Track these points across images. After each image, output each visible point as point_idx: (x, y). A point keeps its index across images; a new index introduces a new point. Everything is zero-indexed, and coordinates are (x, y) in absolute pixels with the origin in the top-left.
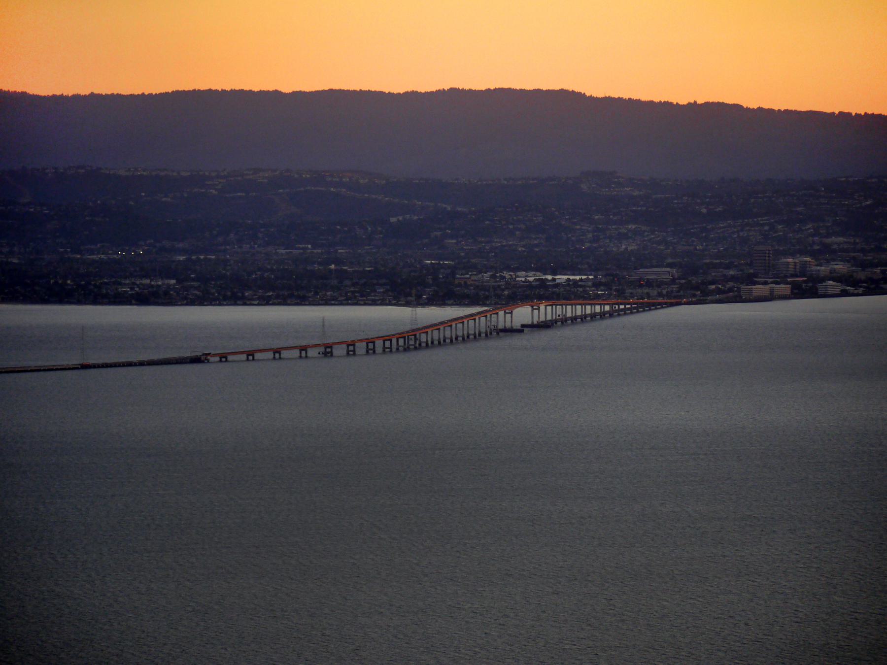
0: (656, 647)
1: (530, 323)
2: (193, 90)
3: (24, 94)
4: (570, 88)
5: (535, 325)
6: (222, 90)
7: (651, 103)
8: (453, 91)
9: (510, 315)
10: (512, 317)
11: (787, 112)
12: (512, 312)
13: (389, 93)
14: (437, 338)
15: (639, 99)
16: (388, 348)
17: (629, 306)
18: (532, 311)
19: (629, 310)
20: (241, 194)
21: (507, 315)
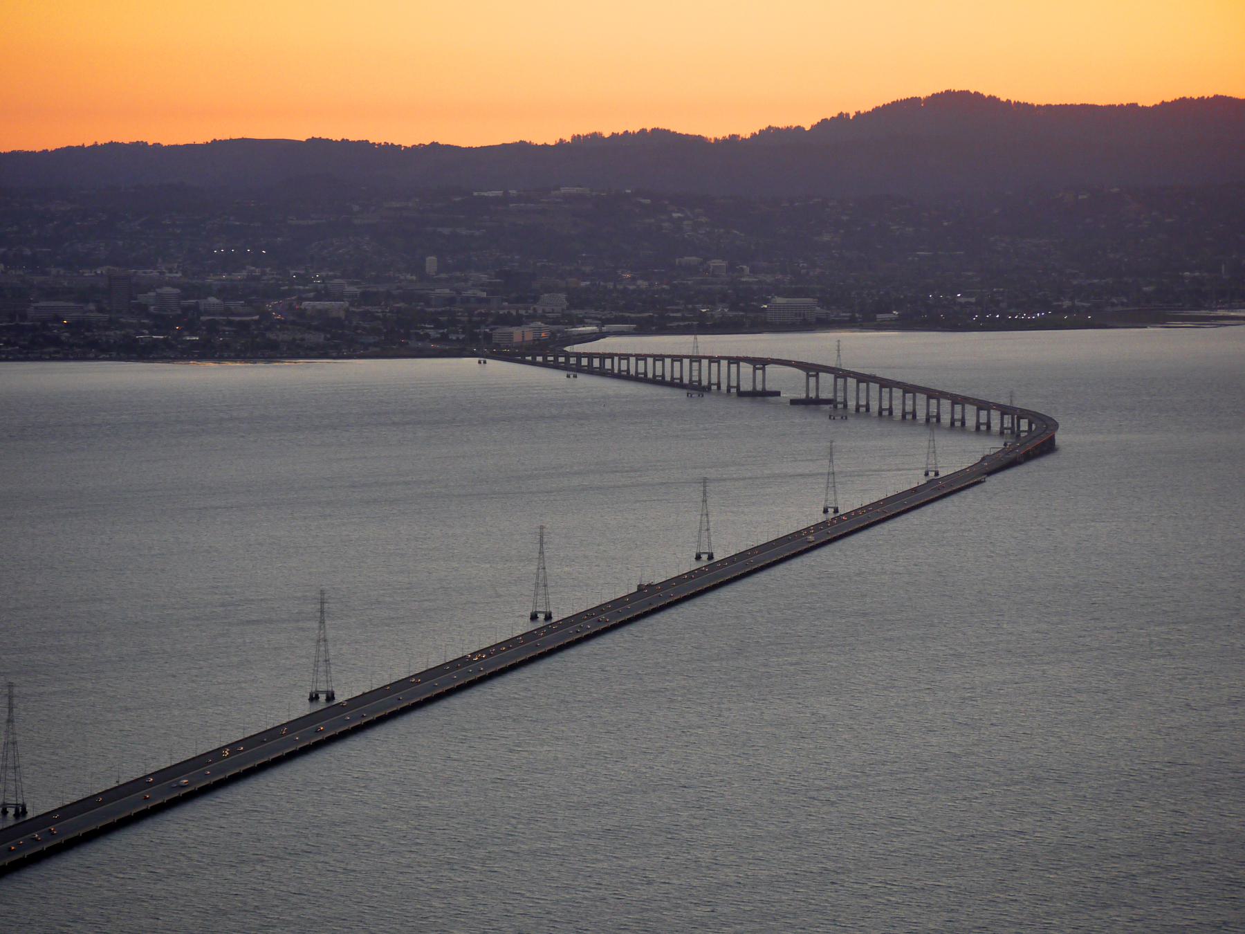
0: (228, 877)
1: (803, 396)
2: (110, 143)
3: (112, 146)
4: (957, 87)
5: (758, 392)
6: (975, 92)
7: (993, 100)
8: (948, 93)
9: (814, 378)
10: (817, 382)
11: (1083, 106)
12: (818, 374)
13: (976, 93)
14: (735, 385)
15: (215, 140)
16: (841, 403)
17: (527, 358)
18: (754, 372)
19: (1031, 426)
20: (643, 201)
21: (712, 364)
